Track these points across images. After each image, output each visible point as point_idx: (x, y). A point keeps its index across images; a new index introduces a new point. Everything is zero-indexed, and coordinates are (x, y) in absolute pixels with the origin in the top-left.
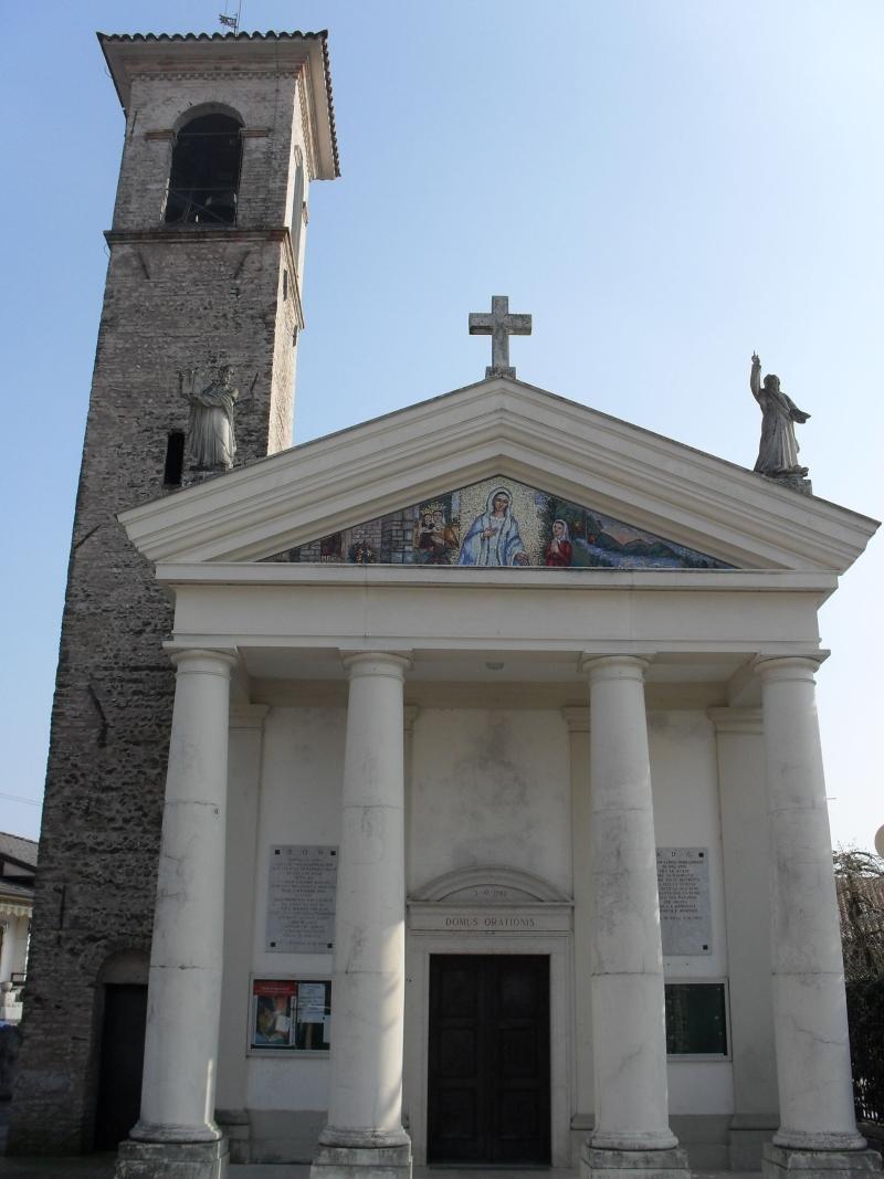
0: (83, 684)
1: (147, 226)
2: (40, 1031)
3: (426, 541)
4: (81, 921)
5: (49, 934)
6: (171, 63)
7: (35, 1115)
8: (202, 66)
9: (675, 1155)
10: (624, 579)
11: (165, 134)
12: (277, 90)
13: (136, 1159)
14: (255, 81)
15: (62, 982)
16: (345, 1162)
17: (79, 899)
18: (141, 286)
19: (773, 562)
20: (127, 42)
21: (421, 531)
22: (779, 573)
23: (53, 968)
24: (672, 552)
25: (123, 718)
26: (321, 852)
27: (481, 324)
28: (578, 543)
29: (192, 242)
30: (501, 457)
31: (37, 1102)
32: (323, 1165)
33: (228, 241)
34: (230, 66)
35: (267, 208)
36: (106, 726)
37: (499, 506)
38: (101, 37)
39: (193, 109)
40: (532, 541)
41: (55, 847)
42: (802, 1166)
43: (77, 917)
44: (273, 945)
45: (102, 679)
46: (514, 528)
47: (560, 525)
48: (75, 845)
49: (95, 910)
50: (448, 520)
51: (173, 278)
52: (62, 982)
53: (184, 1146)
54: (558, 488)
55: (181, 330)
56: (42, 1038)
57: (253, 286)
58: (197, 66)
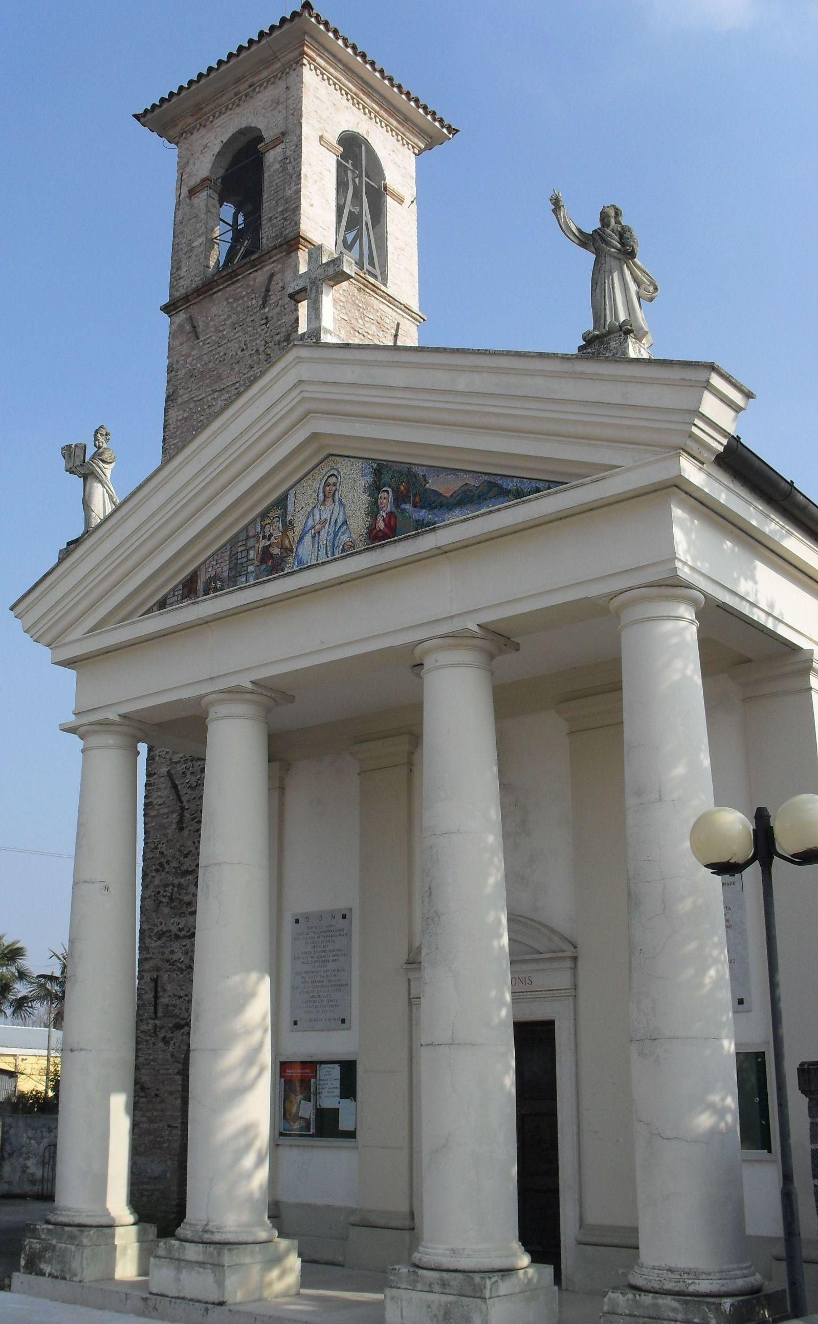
0: (164, 770)
1: (194, 286)
2: (145, 1119)
3: (266, 555)
4: (170, 1008)
5: (148, 1024)
6: (201, 109)
7: (145, 1199)
8: (224, 99)
9: (472, 1279)
10: (427, 542)
11: (205, 183)
12: (287, 88)
13: (36, 1238)
14: (271, 87)
15: (158, 1071)
16: (177, 1256)
17: (168, 987)
18: (194, 349)
19: (596, 464)
20: (157, 111)
21: (261, 546)
22: (603, 478)
23: (151, 1057)
24: (500, 487)
25: (194, 798)
26: (334, 917)
27: (297, 288)
28: (404, 510)
29: (228, 285)
30: (314, 436)
31: (145, 1187)
32: (159, 1257)
33: (256, 271)
34: (246, 85)
35: (285, 219)
36: (183, 809)
37: (329, 494)
38: (136, 116)
39: (226, 145)
40: (358, 524)
41: (150, 937)
42: (620, 1311)
43: (167, 1005)
44: (295, 1023)
45: (179, 762)
46: (341, 513)
47: (385, 494)
48: (164, 933)
49: (180, 997)
50: (284, 525)
51: (217, 331)
52: (158, 1071)
53: (66, 1229)
54: (384, 452)
55: (224, 382)
56: (146, 1126)
57: (278, 309)
58: (220, 101)
